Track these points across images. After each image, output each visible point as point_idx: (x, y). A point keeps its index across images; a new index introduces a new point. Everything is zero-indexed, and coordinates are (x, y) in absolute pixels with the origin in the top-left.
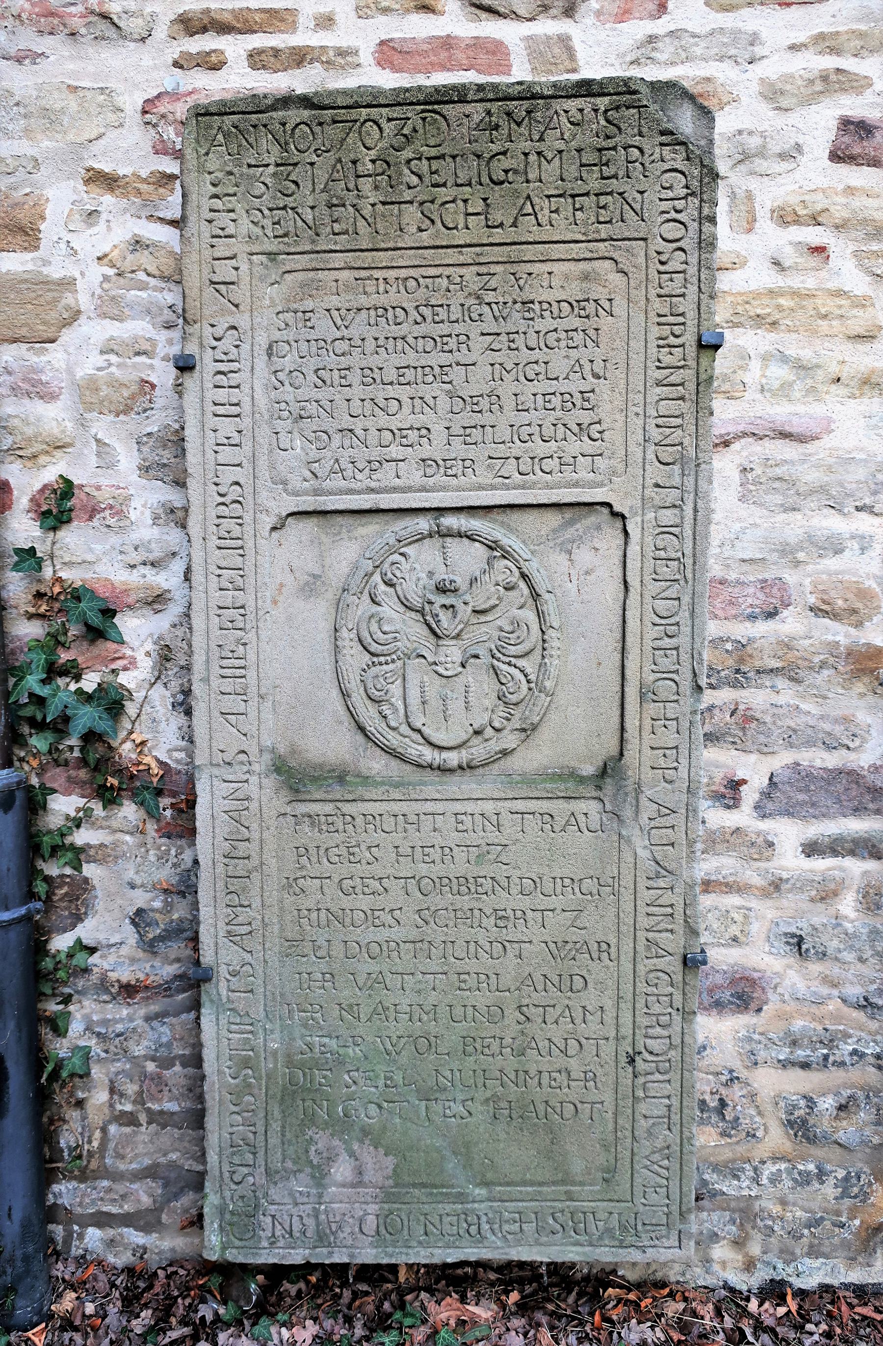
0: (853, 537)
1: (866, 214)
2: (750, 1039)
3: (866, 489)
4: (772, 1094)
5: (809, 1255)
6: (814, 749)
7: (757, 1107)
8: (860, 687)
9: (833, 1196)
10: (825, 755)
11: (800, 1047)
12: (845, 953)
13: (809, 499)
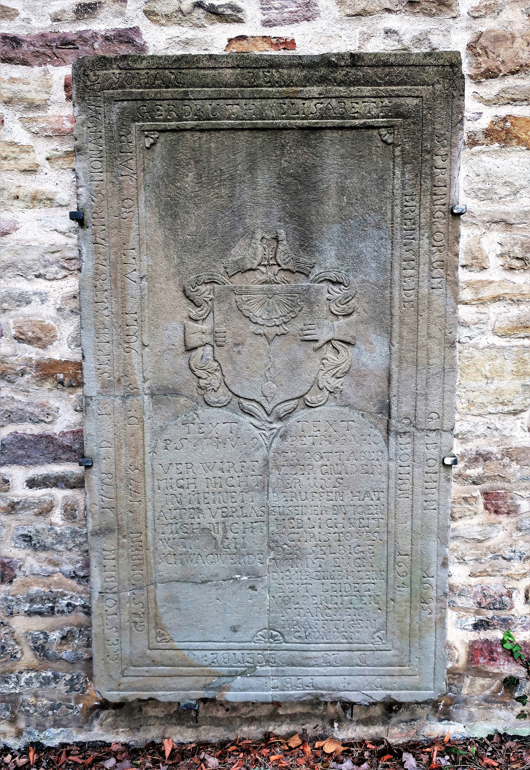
0: (35, 294)
1: (22, 94)
2: (6, 599)
3: (39, 264)
4: (23, 631)
5: (53, 726)
6: (26, 423)
7: (15, 640)
8: (48, 385)
9: (65, 691)
10: (32, 426)
11: (35, 603)
12: (58, 546)
13: (7, 271)
